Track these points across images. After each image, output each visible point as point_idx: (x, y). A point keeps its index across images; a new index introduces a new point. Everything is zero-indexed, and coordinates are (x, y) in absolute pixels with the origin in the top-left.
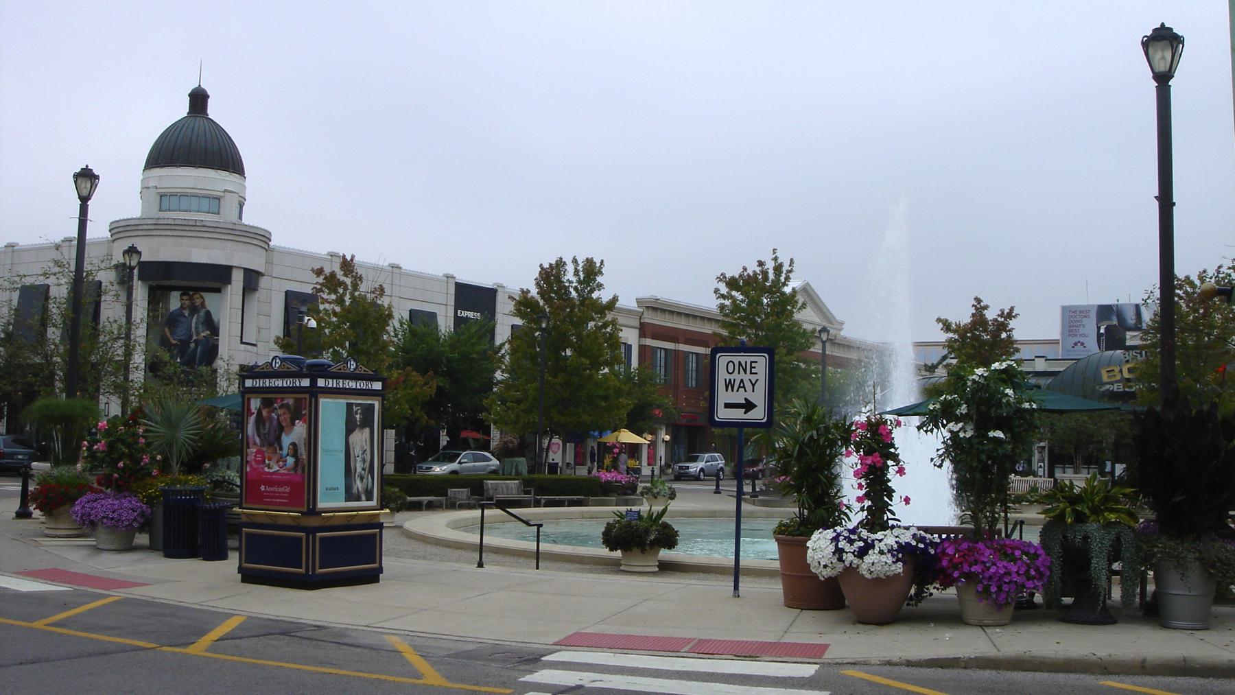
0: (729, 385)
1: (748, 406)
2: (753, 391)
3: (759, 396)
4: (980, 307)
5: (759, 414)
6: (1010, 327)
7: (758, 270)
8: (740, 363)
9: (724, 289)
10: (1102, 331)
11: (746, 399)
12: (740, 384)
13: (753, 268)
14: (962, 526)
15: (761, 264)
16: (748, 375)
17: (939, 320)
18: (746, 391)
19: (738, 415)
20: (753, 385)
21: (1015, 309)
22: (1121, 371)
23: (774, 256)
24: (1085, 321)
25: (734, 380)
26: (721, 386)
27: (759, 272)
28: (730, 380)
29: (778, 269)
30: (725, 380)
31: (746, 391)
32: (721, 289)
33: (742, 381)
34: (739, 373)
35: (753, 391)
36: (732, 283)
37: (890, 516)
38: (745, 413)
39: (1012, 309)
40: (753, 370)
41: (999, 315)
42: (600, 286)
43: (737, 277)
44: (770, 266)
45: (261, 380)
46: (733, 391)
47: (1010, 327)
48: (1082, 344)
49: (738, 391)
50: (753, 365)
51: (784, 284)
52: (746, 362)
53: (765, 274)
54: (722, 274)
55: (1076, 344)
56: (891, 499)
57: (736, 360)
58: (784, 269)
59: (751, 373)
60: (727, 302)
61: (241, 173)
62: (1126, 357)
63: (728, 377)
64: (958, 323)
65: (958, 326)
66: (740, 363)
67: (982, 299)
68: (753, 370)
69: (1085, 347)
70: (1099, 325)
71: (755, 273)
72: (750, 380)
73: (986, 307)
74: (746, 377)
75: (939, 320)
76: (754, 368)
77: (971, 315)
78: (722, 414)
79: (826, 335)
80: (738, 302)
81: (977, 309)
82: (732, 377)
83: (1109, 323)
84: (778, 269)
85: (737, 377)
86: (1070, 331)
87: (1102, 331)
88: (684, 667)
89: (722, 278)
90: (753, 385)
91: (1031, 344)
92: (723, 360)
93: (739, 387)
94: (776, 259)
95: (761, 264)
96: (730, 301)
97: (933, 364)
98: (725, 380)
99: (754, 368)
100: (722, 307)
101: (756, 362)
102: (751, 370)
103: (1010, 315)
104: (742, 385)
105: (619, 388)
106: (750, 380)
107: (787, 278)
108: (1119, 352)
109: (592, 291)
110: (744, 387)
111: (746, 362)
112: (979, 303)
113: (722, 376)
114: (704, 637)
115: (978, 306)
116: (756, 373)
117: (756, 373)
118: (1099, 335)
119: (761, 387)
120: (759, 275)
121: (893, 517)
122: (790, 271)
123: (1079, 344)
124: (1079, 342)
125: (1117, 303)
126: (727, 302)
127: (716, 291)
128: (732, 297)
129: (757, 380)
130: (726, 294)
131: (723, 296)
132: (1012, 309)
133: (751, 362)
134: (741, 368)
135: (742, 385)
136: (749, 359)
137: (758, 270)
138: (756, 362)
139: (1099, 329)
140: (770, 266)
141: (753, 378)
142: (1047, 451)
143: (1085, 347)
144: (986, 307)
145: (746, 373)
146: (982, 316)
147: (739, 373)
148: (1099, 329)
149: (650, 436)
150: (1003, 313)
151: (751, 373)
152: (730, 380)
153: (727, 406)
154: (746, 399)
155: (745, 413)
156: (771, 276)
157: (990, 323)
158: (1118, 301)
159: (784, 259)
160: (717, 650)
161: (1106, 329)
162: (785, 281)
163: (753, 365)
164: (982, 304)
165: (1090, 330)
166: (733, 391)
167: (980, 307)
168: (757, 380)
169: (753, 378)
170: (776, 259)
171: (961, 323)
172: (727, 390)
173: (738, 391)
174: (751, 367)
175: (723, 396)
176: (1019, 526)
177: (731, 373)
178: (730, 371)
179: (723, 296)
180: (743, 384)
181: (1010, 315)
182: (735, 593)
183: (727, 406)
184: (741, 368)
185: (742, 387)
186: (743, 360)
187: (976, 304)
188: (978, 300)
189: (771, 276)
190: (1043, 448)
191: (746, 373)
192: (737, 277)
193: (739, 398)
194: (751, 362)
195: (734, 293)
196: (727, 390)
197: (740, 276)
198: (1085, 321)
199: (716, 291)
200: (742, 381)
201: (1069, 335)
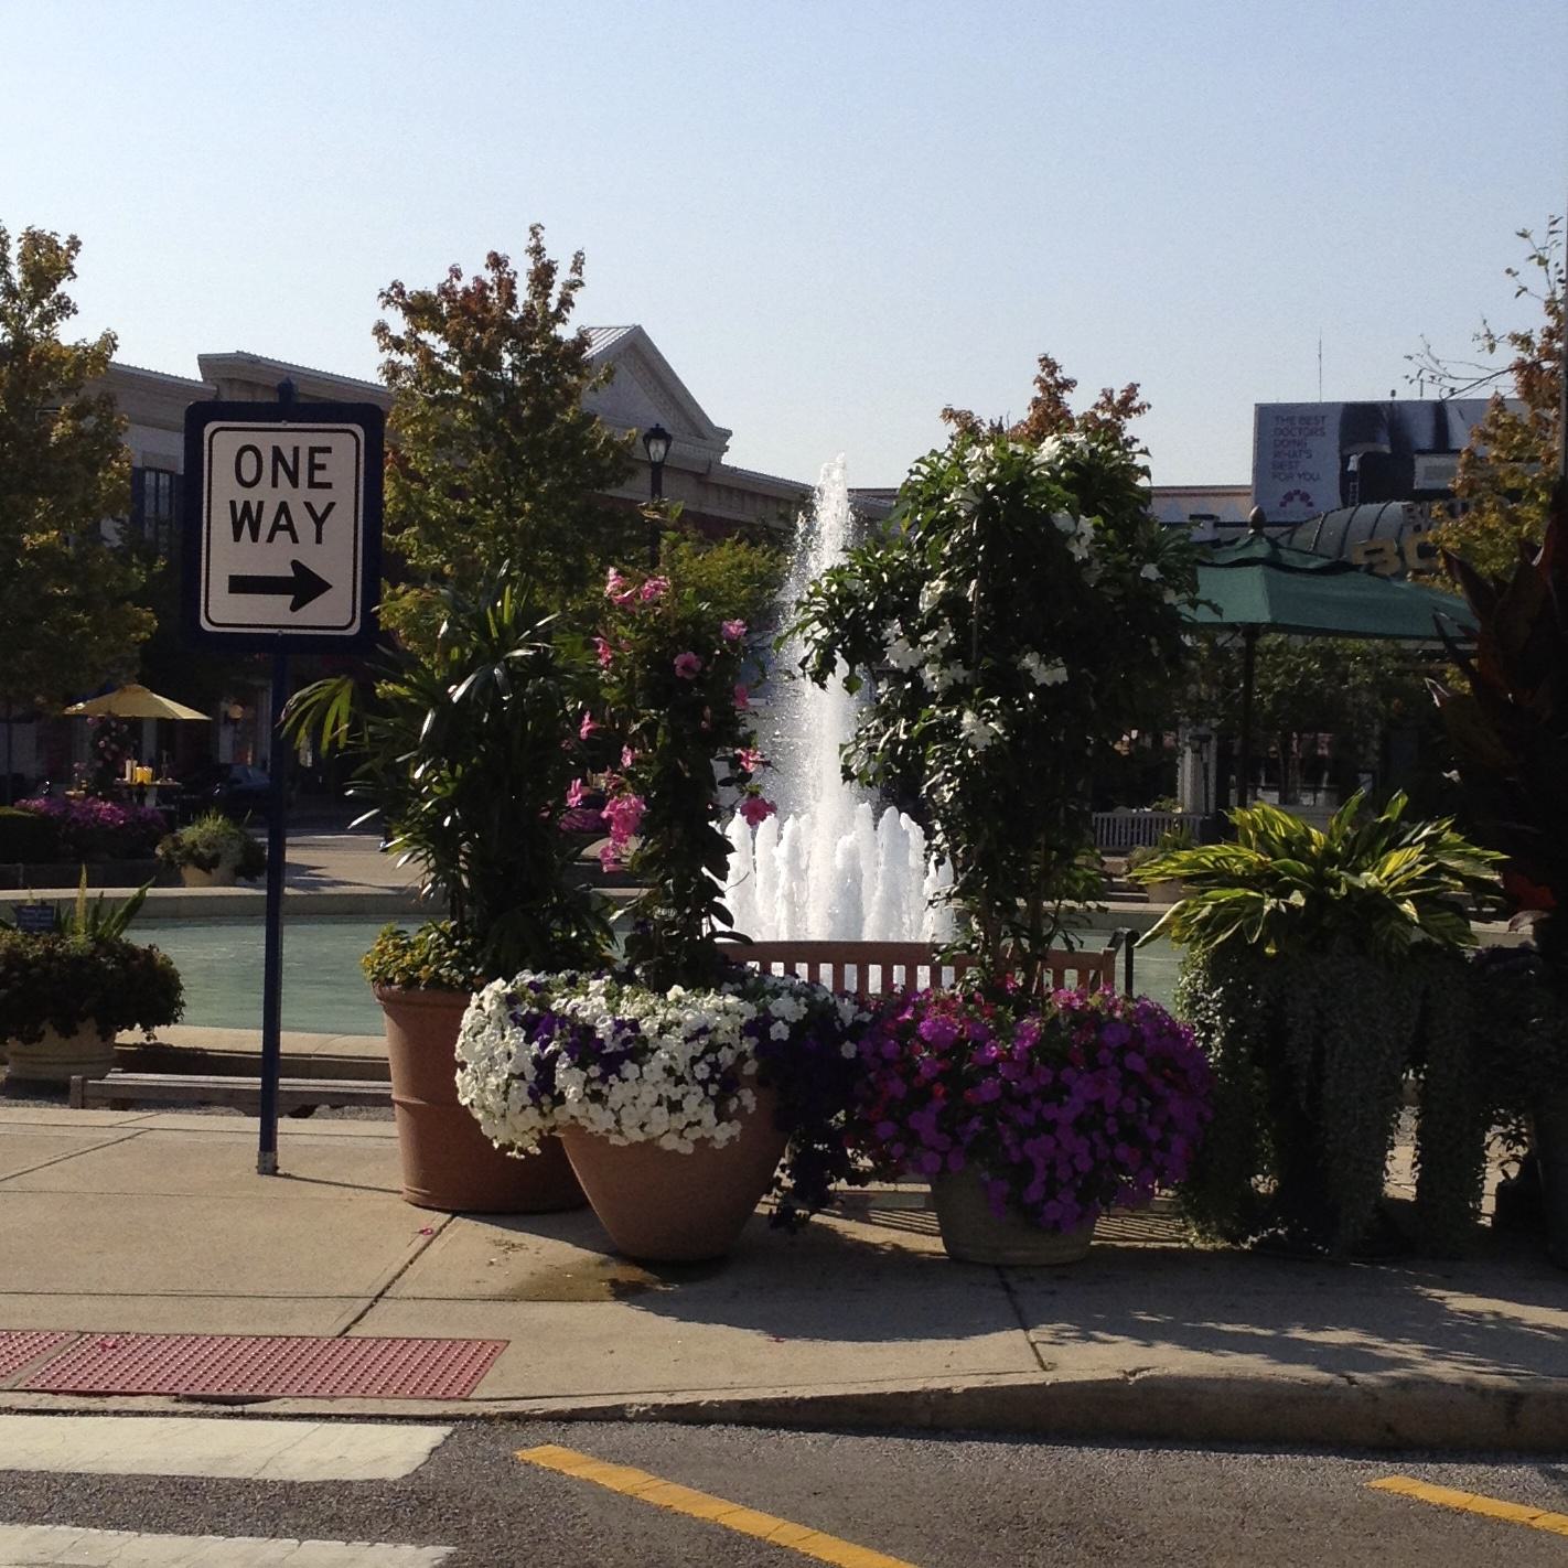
0: (245, 520)
1: (304, 585)
2: (319, 540)
3: (336, 559)
4: (1053, 388)
5: (333, 612)
6: (1127, 434)
7: (489, 276)
8: (277, 454)
9: (399, 325)
10: (1353, 466)
11: (296, 565)
12: (277, 519)
13: (475, 269)
15: (496, 261)
16: (304, 492)
17: (950, 414)
18: (295, 540)
19: (271, 611)
20: (319, 522)
21: (1138, 390)
22: (1401, 553)
23: (533, 243)
24: (1313, 443)
25: (261, 504)
26: (219, 523)
27: (491, 284)
28: (247, 504)
29: (543, 276)
30: (233, 504)
31: (295, 540)
32: (390, 326)
33: (283, 508)
34: (275, 484)
35: (319, 540)
36: (420, 309)
37: (720, 927)
38: (295, 607)
39: (1132, 390)
40: (319, 476)
41: (1097, 406)
42: (65, 307)
43: (435, 293)
44: (521, 267)
46: (255, 538)
47: (1127, 434)
48: (1305, 497)
49: (270, 539)
50: (319, 458)
51: (558, 317)
52: (296, 450)
53: (506, 286)
54: (394, 285)
55: (1289, 497)
56: (722, 870)
57: (265, 441)
58: (562, 276)
59: (312, 484)
60: (407, 360)
62: (1413, 517)
63: (242, 495)
64: (996, 424)
65: (998, 430)
66: (277, 454)
67: (1059, 362)
68: (319, 476)
69: (1311, 505)
70: (1346, 452)
71: (482, 286)
72: (308, 505)
73: (1068, 385)
74: (297, 497)
76: (322, 467)
77: (1029, 403)
78: (223, 609)
79: (662, 448)
80: (436, 359)
81: (1045, 388)
82: (254, 496)
83: (1370, 447)
84: (543, 276)
85: (267, 496)
87: (1353, 466)
89: (395, 295)
90: (319, 522)
92: (223, 444)
93: (276, 527)
94: (537, 251)
95: (496, 261)
96: (414, 356)
98: (233, 504)
99: (322, 467)
100: (393, 371)
101: (328, 450)
102: (311, 476)
103: (1126, 405)
104: (283, 521)
106: (308, 505)
107: (566, 302)
108: (1396, 506)
109: (47, 318)
110: (290, 527)
111: (296, 450)
112: (1051, 374)
113: (222, 491)
115: (1050, 381)
116: (328, 486)
117: (328, 486)
118: (1346, 477)
119: (343, 527)
120: (491, 289)
121: (726, 929)
122: (574, 285)
123: (1297, 498)
124: (1298, 492)
125: (1390, 399)
126: (407, 360)
127: (381, 330)
128: (419, 345)
129: (331, 505)
130: (403, 337)
131: (398, 344)
132: (1132, 390)
133: (313, 451)
134: (280, 467)
135: (283, 521)
136: (306, 441)
137: (489, 276)
138: (328, 450)
139: (1345, 461)
140: (521, 267)
141: (320, 500)
142: (1213, 750)
143: (1311, 505)
144: (1068, 385)
145: (295, 484)
146: (1057, 403)
147: (275, 484)
148: (1345, 461)
149: (240, 709)
150: (1109, 400)
151: (312, 484)
152: (247, 504)
153: (240, 585)
154: (296, 565)
155: (295, 607)
156: (523, 293)
157: (1077, 423)
158: (1393, 393)
159: (559, 254)
160: (123, 1381)
161: (1361, 462)
162: (558, 310)
163: (319, 458)
164: (1058, 375)
165: (1325, 461)
166: (255, 538)
167: (1053, 388)
168: (331, 505)
169: (320, 500)
170: (537, 251)
171: (1004, 422)
172: (237, 537)
173: (270, 539)
174: (313, 467)
175: (225, 555)
176: (1124, 946)
177: (250, 485)
178: (248, 476)
179: (398, 344)
180: (289, 519)
181: (1126, 405)
182: (262, 1160)
183: (240, 585)
184: (280, 467)
185: (283, 528)
186: (286, 442)
187: (1043, 375)
188: (1049, 365)
189: (523, 293)
190: (1205, 739)
191: (295, 484)
192: (435, 293)
193: (273, 559)
194: (313, 451)
195: (424, 336)
196: (237, 537)
197: (443, 291)
198: (1313, 443)
199: (381, 330)
200: (283, 508)
201: (1275, 476)
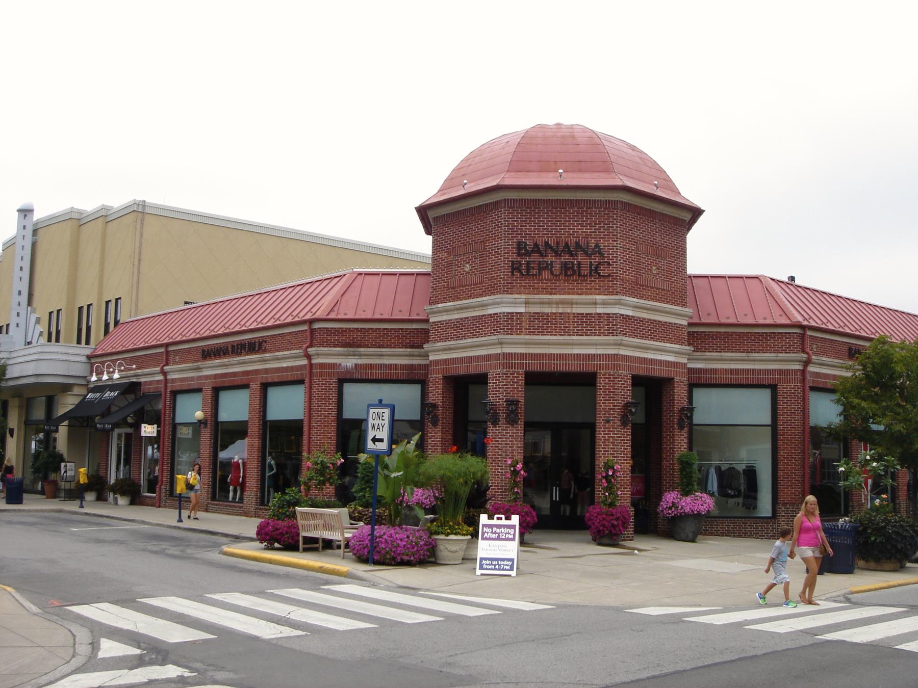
14: (889, 492)
17: (25, 218)
20: (383, 427)
45: (399, 378)
50: (383, 414)
59: (382, 420)
61: (687, 216)
75: (25, 218)
86: (250, 405)
88: (252, 605)
90: (383, 427)
91: (652, 214)
93: (378, 428)
97: (903, 342)
105: (572, 307)
110: (379, 428)
114: (153, 678)
141: (383, 422)
163: (383, 414)
169: (383, 422)
174: (383, 416)
